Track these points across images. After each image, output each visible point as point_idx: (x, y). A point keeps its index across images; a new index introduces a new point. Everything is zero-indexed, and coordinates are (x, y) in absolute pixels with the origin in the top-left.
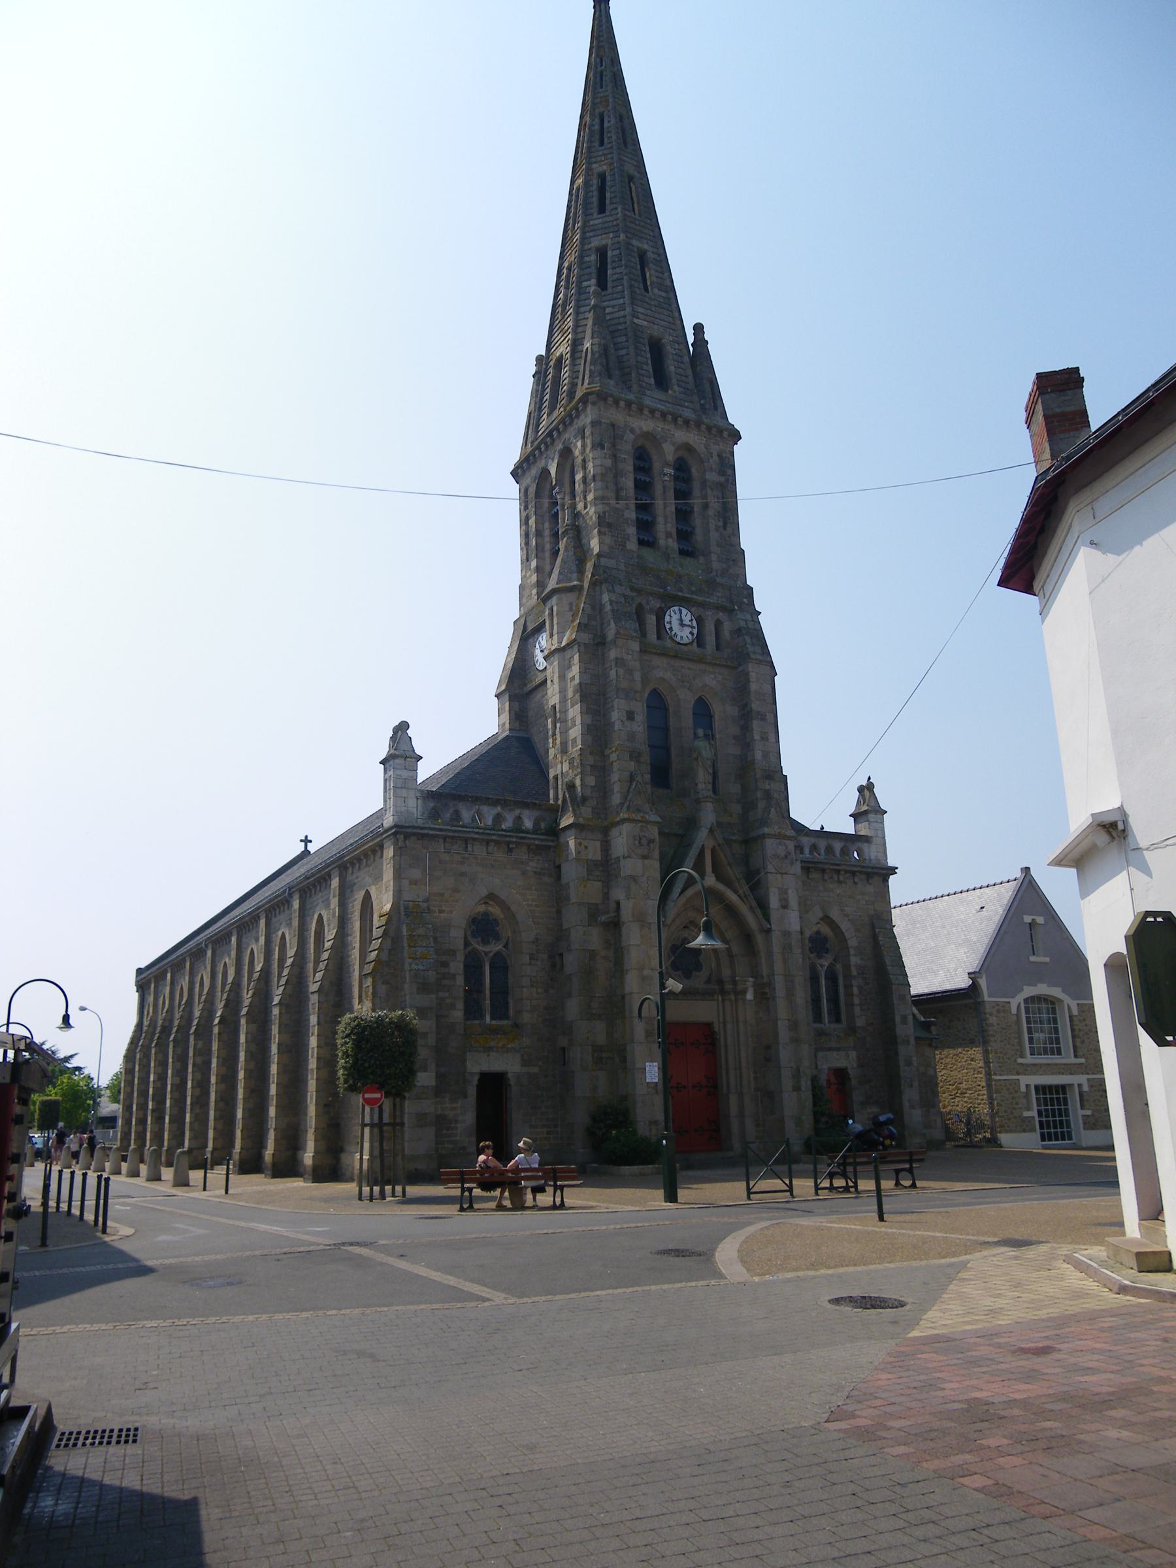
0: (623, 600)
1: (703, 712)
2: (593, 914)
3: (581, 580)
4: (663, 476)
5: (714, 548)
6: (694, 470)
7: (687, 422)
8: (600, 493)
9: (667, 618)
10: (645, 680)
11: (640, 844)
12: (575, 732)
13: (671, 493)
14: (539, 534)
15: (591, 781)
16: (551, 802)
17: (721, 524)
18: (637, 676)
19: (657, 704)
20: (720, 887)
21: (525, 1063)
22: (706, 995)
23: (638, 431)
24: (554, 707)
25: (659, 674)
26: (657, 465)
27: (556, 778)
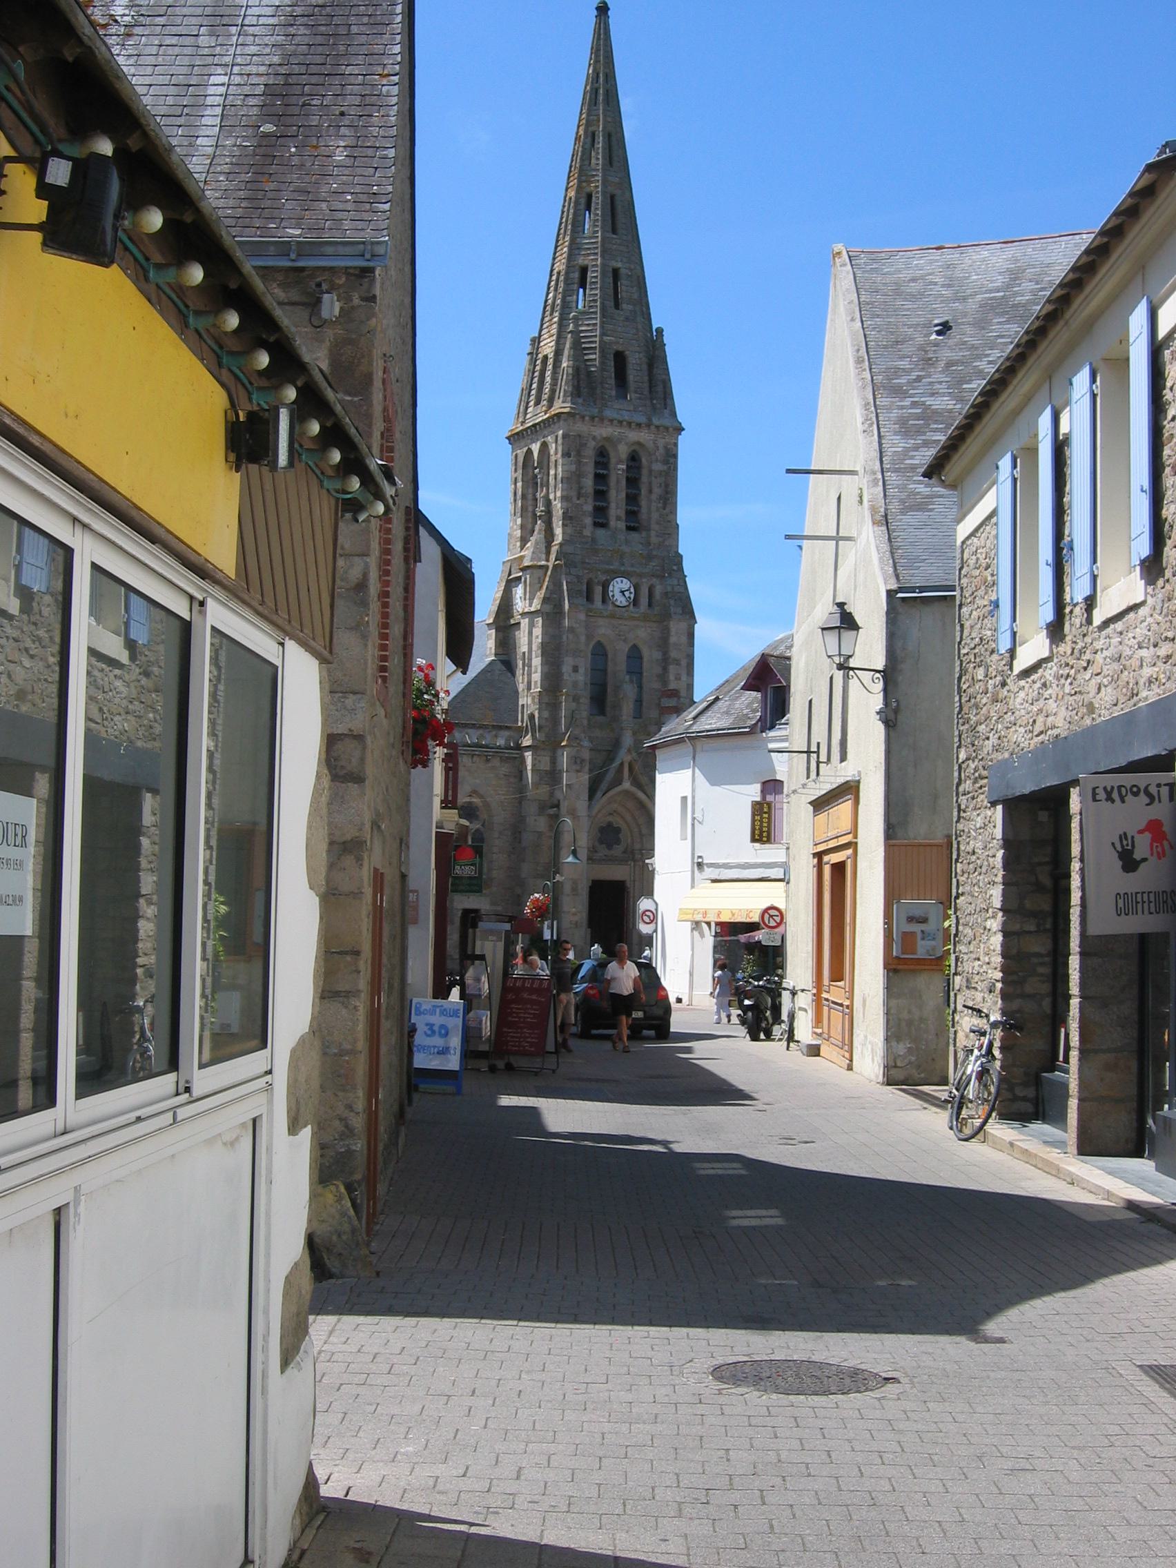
0: (576, 580)
1: (635, 655)
2: (543, 807)
3: (547, 560)
4: (619, 469)
5: (654, 526)
6: (644, 460)
7: (639, 425)
8: (565, 493)
9: (611, 588)
10: (589, 637)
11: (576, 762)
12: (537, 677)
13: (624, 482)
14: (524, 497)
15: (546, 714)
16: (520, 724)
17: (660, 505)
18: (583, 638)
19: (600, 652)
20: (634, 789)
21: (493, 904)
22: (622, 861)
23: (599, 438)
24: (524, 653)
25: (602, 631)
26: (613, 460)
27: (523, 705)
